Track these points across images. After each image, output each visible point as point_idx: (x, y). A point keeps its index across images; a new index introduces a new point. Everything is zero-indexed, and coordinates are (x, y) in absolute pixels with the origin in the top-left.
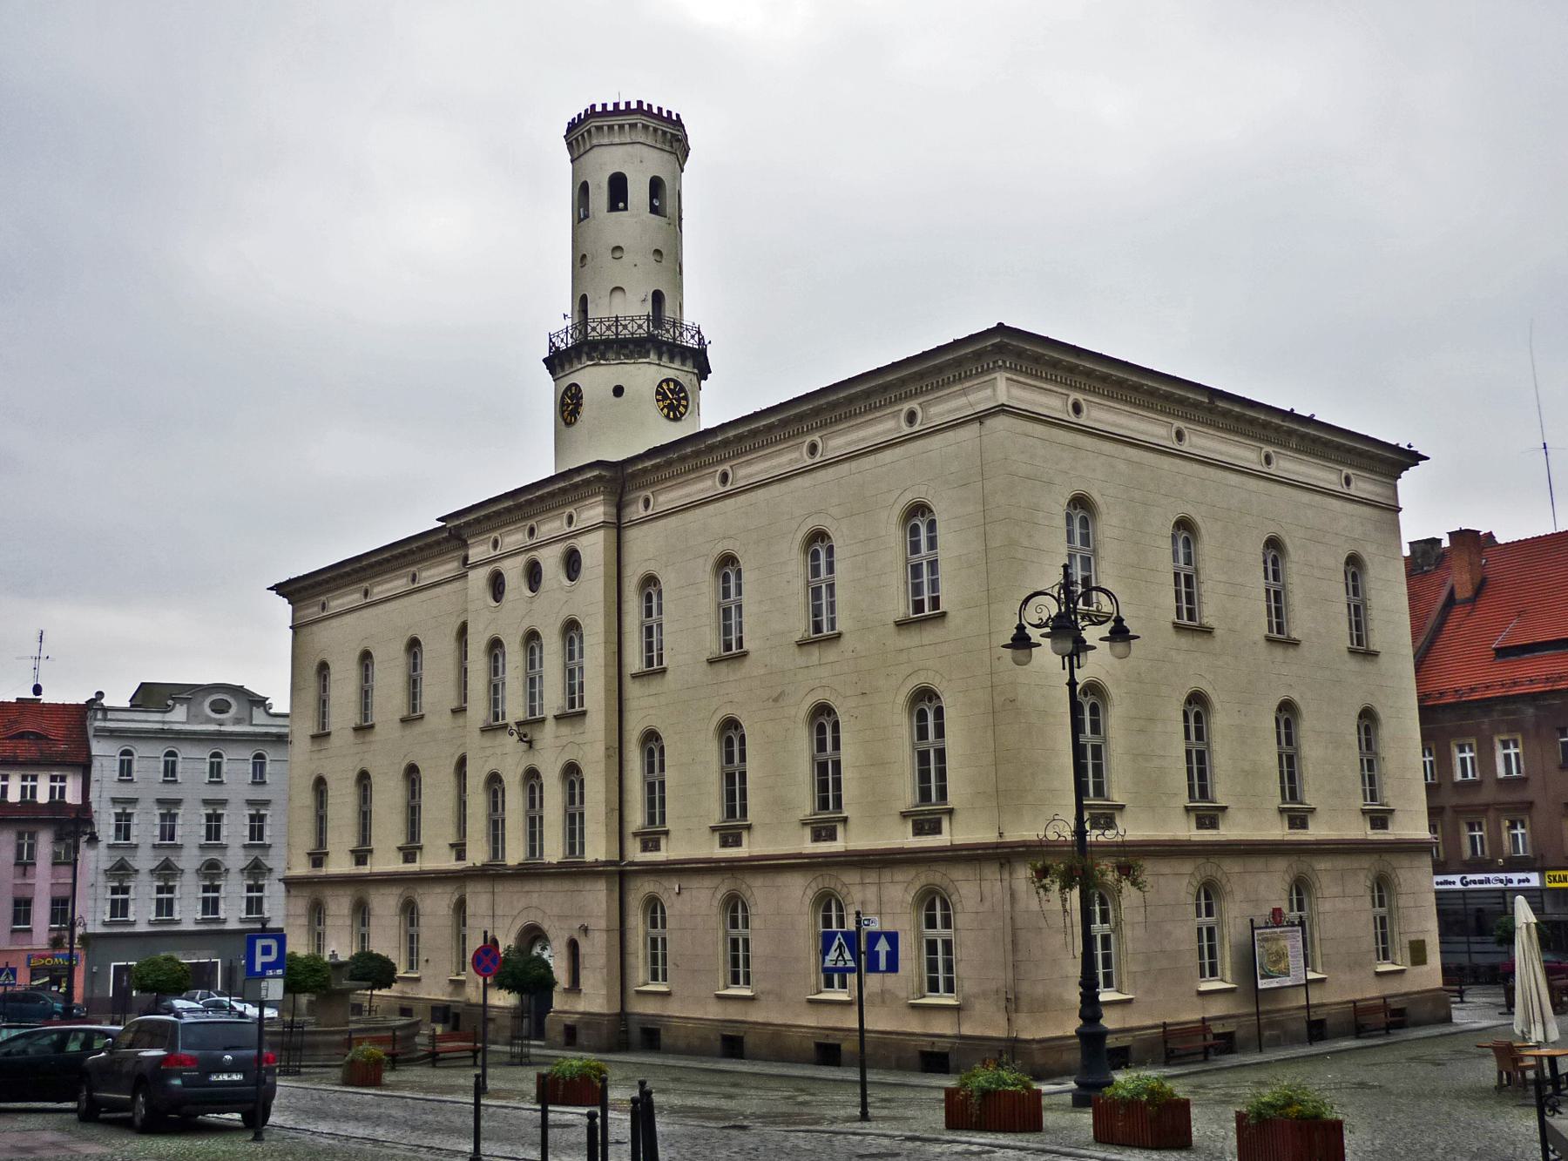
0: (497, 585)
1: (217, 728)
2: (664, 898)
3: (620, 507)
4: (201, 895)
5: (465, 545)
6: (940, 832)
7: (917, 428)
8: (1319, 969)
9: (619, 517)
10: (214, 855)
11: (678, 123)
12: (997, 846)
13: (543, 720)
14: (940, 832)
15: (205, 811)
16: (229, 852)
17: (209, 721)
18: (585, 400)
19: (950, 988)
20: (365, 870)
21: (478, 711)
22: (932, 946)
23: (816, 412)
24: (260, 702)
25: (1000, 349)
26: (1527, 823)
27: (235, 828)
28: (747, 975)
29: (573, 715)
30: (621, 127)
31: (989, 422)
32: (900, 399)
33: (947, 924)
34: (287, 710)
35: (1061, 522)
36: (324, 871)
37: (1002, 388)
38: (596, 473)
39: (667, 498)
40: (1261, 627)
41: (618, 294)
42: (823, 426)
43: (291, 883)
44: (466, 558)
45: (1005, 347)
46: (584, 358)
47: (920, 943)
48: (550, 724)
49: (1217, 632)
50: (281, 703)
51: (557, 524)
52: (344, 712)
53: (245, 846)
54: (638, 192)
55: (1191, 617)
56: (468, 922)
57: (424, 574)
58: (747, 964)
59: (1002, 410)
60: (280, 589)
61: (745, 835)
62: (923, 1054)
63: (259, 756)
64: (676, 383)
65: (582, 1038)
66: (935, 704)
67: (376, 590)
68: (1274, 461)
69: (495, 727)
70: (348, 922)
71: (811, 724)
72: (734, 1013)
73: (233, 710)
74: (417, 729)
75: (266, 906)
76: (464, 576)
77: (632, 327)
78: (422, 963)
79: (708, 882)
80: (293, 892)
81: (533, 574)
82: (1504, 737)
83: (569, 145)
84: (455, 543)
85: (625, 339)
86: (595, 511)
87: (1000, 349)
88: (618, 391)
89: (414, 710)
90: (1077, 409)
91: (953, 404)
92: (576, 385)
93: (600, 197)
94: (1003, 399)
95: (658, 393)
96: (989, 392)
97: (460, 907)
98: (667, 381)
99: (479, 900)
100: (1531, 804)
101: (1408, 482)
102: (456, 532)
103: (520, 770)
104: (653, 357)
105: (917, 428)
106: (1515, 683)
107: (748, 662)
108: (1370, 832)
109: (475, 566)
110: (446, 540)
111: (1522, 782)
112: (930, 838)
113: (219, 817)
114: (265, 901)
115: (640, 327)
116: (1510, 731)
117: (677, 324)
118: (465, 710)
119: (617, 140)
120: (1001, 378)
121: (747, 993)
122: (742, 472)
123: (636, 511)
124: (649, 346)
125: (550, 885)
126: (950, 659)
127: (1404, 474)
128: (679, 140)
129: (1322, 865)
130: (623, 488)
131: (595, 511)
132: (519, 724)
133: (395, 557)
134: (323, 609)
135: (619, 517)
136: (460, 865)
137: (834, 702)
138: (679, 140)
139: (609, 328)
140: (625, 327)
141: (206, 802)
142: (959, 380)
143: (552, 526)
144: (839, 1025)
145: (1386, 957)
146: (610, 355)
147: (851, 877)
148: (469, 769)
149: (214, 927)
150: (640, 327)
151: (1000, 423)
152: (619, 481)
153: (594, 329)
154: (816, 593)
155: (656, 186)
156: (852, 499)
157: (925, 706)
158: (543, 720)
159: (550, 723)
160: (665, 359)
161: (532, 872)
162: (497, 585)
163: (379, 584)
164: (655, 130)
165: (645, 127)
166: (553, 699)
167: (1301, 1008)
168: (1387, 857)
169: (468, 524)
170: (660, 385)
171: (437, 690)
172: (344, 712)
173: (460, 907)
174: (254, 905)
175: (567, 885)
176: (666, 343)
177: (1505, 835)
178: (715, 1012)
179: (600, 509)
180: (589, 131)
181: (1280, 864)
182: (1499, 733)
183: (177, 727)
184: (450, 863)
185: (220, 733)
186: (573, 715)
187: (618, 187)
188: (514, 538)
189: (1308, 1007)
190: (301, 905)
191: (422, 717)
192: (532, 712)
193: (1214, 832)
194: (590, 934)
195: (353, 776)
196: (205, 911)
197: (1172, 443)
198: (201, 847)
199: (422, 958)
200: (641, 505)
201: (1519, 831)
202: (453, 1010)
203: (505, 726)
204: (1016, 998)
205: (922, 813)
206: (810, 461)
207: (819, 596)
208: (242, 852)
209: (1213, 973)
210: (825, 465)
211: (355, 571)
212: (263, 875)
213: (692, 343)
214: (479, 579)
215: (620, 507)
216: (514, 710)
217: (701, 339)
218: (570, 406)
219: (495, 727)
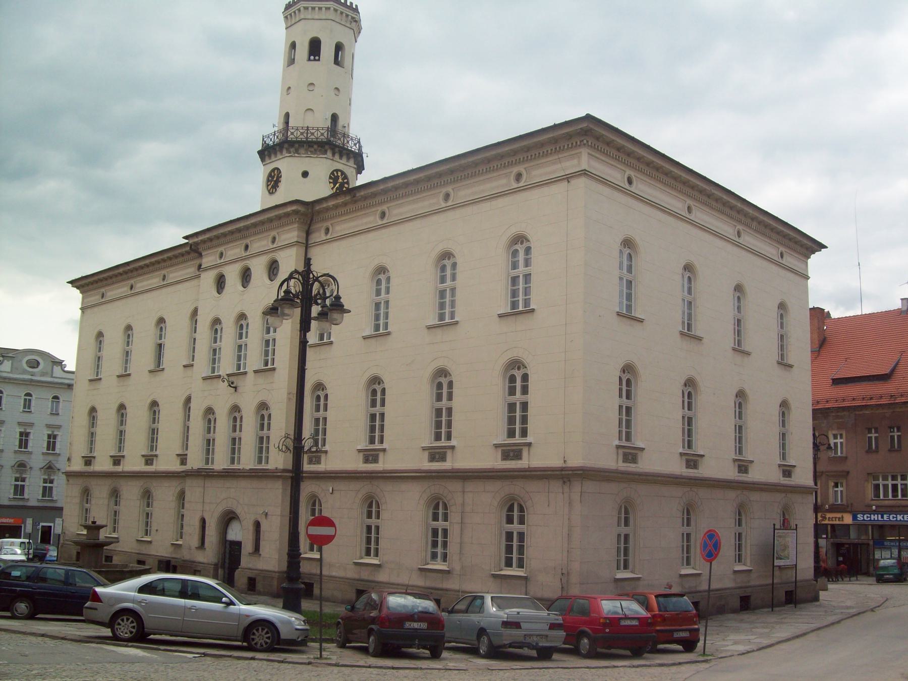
0: (220, 283)
1: (30, 377)
2: (321, 496)
3: (308, 233)
4: (14, 483)
5: (200, 255)
6: (521, 459)
7: (521, 184)
8: (697, 567)
9: (307, 240)
10: (22, 457)
11: (356, 10)
12: (562, 469)
13: (245, 373)
14: (521, 459)
15: (19, 429)
16: (33, 456)
17: (25, 372)
18: (283, 179)
19: (521, 565)
20: (119, 469)
21: (202, 367)
22: (509, 536)
23: (452, 172)
24: (60, 363)
25: (586, 132)
26: (844, 485)
27: (37, 442)
28: (377, 550)
29: (267, 369)
30: (320, 9)
31: (574, 182)
32: (511, 164)
33: (522, 521)
34: (74, 369)
35: (617, 254)
36: (91, 469)
37: (584, 159)
38: (294, 208)
39: (341, 228)
40: (730, 342)
41: (309, 113)
42: (456, 181)
43: (69, 475)
44: (200, 266)
45: (590, 133)
46: (284, 151)
47: (501, 534)
48: (251, 376)
49: (704, 340)
50: (71, 366)
51: (264, 243)
52: (112, 365)
53: (43, 454)
54: (327, 51)
55: (688, 330)
56: (186, 505)
57: (171, 275)
58: (377, 543)
59: (584, 173)
60: (72, 282)
61: (381, 455)
62: (160, 562)
63: (56, 397)
64: (343, 173)
65: (259, 586)
66: (522, 371)
67: (139, 285)
68: (742, 235)
69: (212, 378)
70: (106, 502)
71: (433, 381)
72: (365, 575)
73: (41, 367)
74: (161, 377)
75: (54, 493)
76: (198, 277)
77: (317, 134)
78: (153, 532)
79: (355, 485)
80: (71, 481)
81: (246, 276)
82: (834, 432)
83: (286, 17)
84: (193, 255)
85: (312, 142)
86: (292, 234)
87: (586, 132)
88: (305, 174)
89: (159, 366)
90: (630, 181)
91: (548, 169)
92: (278, 169)
93: (303, 50)
94: (584, 166)
95: (330, 177)
96: (575, 162)
97: (182, 496)
98: (337, 171)
99: (194, 490)
100: (848, 472)
101: (815, 259)
102: (194, 248)
103: (228, 406)
104: (329, 154)
105: (521, 184)
106: (854, 399)
107: (390, 338)
108: (782, 478)
109: (206, 269)
110: (188, 253)
111: (844, 459)
112: (513, 462)
113: (27, 434)
114: (54, 489)
115: (322, 134)
116: (839, 428)
117: (345, 135)
118: (192, 365)
119: (317, 17)
120: (584, 153)
121: (376, 562)
122: (396, 211)
123: (318, 236)
124: (327, 147)
125: (243, 483)
126: (534, 342)
127: (812, 256)
128: (356, 21)
129: (755, 496)
130: (312, 220)
131: (292, 234)
132: (229, 375)
133: (153, 264)
134: (103, 297)
135: (307, 240)
136: (183, 468)
137: (451, 367)
138: (356, 21)
139: (302, 134)
140: (313, 134)
141: (20, 424)
142: (556, 151)
143: (260, 244)
144: (440, 586)
145: (688, 563)
146: (302, 151)
147: (455, 486)
148: (193, 405)
149: (21, 503)
150: (322, 134)
151: (582, 182)
152: (308, 215)
153: (292, 133)
154: (514, 280)
155: (339, 47)
156: (476, 231)
157: (376, 387)
158: (245, 373)
159: (251, 375)
160: (337, 157)
161: (228, 475)
162: (220, 283)
163: (141, 281)
164: (342, 13)
165: (336, 10)
166: (254, 360)
167: (705, 591)
168: (789, 495)
169: (204, 242)
170: (332, 173)
171: (175, 354)
172: (112, 365)
173: (182, 496)
174: (47, 491)
175: (255, 483)
176: (338, 146)
177: (831, 491)
178: (351, 573)
179: (295, 233)
180: (299, 10)
181: (732, 494)
182: (833, 429)
183: (5, 375)
184: (176, 467)
185: (32, 381)
186: (267, 369)
187: (315, 48)
188: (234, 251)
189: (709, 590)
190: (75, 490)
191: (163, 369)
192: (239, 367)
193: (695, 471)
194: (269, 517)
195: (115, 406)
196: (15, 493)
197: (685, 213)
198: (16, 452)
199: (154, 528)
200: (323, 231)
201: (840, 489)
202: (173, 563)
203: (219, 377)
204: (568, 573)
205: (509, 445)
206: (444, 205)
207: (445, 300)
208: (41, 457)
209: (688, 563)
210: (453, 208)
211: (126, 273)
212: (54, 473)
213: (355, 149)
214: (208, 278)
215: (308, 233)
216: (226, 366)
217: (360, 147)
218: (273, 181)
219: (212, 378)
